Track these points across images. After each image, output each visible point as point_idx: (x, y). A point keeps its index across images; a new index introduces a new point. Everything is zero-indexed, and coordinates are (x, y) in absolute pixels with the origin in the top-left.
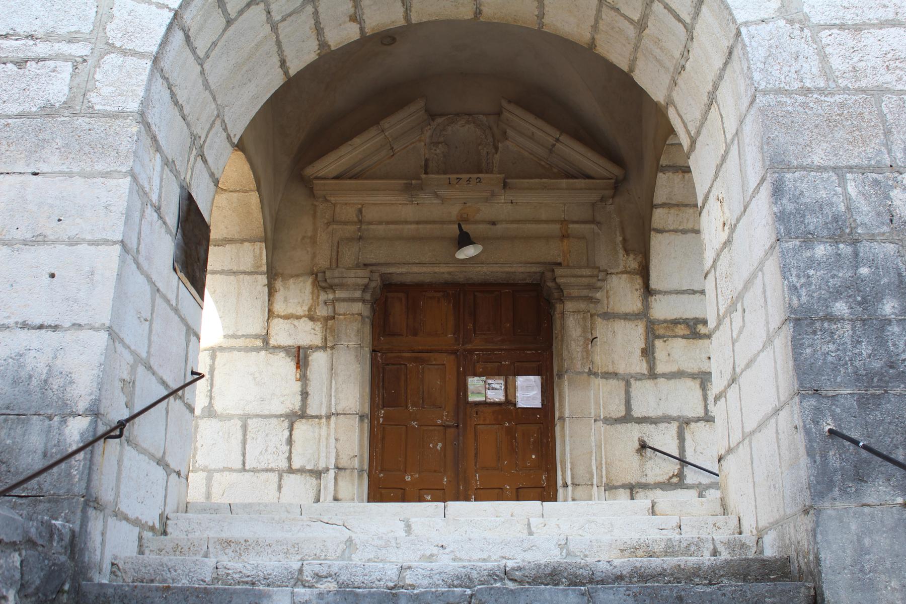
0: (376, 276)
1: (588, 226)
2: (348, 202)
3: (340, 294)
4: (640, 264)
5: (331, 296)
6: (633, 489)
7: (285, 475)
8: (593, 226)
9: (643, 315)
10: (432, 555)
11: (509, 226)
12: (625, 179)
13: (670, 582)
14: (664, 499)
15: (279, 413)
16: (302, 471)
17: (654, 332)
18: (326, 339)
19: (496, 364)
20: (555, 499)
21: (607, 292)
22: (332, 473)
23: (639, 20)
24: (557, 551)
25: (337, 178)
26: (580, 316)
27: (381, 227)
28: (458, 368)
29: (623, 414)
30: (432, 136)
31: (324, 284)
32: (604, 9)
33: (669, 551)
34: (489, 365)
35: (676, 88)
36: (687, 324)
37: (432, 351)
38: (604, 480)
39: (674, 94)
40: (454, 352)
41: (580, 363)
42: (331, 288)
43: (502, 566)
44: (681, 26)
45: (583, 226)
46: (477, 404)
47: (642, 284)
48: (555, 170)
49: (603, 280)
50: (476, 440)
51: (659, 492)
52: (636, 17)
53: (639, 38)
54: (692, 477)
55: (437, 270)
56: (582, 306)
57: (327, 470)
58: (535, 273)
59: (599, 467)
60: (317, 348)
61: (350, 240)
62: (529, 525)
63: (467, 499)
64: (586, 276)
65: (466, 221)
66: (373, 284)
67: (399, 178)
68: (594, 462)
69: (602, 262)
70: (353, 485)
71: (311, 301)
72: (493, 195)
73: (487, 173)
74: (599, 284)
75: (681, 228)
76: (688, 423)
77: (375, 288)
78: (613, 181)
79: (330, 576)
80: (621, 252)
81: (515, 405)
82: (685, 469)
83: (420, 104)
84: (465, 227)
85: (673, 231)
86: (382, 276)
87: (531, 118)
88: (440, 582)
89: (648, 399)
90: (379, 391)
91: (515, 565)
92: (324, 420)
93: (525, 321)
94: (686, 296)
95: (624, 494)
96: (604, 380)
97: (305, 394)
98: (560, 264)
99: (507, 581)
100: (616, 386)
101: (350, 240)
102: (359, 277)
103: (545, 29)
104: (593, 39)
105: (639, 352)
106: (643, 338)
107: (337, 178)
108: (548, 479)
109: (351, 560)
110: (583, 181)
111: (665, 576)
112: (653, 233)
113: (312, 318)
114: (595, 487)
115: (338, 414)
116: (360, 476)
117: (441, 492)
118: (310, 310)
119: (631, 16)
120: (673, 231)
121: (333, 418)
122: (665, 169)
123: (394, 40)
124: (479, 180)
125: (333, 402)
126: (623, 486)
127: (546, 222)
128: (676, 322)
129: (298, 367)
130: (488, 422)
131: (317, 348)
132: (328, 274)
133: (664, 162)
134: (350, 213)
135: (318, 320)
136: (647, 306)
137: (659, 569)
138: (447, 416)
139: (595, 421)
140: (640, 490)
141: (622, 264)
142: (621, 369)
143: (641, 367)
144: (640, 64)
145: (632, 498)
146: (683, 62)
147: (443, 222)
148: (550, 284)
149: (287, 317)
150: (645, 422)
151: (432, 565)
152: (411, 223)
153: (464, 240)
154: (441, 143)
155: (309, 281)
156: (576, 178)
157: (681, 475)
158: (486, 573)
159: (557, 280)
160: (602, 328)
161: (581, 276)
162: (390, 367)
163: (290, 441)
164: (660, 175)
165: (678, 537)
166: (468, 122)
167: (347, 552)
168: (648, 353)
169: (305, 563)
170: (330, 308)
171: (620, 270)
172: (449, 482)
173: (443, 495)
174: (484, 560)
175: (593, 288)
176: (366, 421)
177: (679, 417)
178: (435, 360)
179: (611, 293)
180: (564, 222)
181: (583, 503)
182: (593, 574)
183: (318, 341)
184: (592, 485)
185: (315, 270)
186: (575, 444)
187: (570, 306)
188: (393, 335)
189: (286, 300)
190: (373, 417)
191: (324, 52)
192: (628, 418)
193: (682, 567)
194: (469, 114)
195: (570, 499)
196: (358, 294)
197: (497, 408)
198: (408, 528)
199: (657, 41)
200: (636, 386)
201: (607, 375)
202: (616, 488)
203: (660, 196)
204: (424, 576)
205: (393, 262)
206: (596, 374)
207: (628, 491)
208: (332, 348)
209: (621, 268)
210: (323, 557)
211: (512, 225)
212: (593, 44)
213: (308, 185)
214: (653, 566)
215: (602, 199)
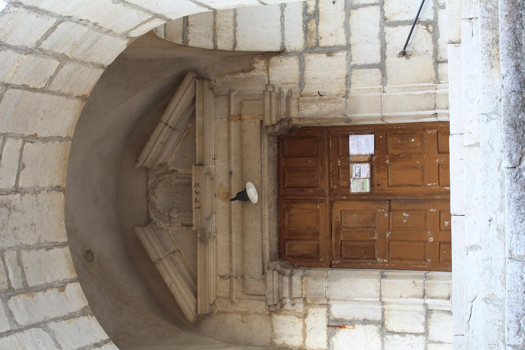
0: (272, 265)
1: (232, 100)
2: (214, 287)
3: (286, 294)
4: (261, 59)
5: (288, 300)
6: (438, 61)
7: (429, 338)
8: (232, 96)
9: (300, 56)
10: (498, 229)
11: (232, 161)
12: (195, 71)
13: (521, 24)
14: (446, 33)
15: (380, 343)
16: (426, 325)
17: (313, 47)
18: (322, 305)
19: (341, 170)
20: (447, 123)
21: (283, 84)
22: (428, 301)
23: (59, 61)
24: (493, 123)
25: (196, 295)
26: (301, 104)
27: (234, 260)
28: (344, 200)
29: (378, 70)
30: (164, 222)
31: (279, 306)
32: (51, 88)
33: (493, 26)
34: (341, 176)
35: (114, 30)
36: (307, 21)
37: (331, 221)
38: (431, 84)
39: (119, 32)
40: (331, 203)
41: (338, 105)
42: (281, 300)
43: (508, 170)
44: (60, 26)
45: (232, 104)
46: (372, 185)
47: (276, 57)
48: (190, 125)
49: (274, 87)
50: (401, 186)
51: (441, 41)
52: (56, 63)
53: (74, 60)
54: (427, 15)
55: (267, 217)
56: (294, 103)
57: (425, 304)
58: (269, 141)
59: (421, 88)
60: (328, 311)
61: (244, 285)
62: (470, 146)
63: (448, 193)
64: (271, 101)
65: (229, 194)
66: (279, 267)
67: (197, 244)
68: (417, 93)
69: (259, 88)
70: (437, 278)
71: (292, 316)
72: (209, 174)
73: (191, 179)
74: (277, 90)
75: (232, 27)
76: (385, 19)
77: (281, 266)
78: (197, 81)
79: (518, 321)
80: (252, 73)
81: (372, 155)
82: (421, 20)
83: (139, 230)
84: (234, 196)
85: (235, 33)
86: (272, 260)
87: (150, 144)
88: (523, 224)
89: (366, 51)
90: (362, 263)
91: (507, 159)
92: (386, 307)
93: (306, 150)
94: (286, 23)
95: (442, 68)
96: (352, 85)
97: (365, 322)
98: (262, 121)
99: (521, 167)
100: (357, 76)
101: (244, 285)
102: (273, 278)
103: (71, 135)
104: (78, 97)
105: (330, 59)
106: (318, 56)
107: (196, 295)
108: (431, 129)
109: (504, 299)
110: (197, 104)
111: (515, 28)
112: (237, 49)
113: (305, 316)
114: (437, 91)
115: (381, 296)
116: (430, 278)
117: (442, 213)
118: (299, 317)
119: (56, 67)
120: (235, 33)
121: (384, 300)
122: (185, 41)
123: (89, 252)
124: (197, 185)
125: (371, 299)
126: (436, 69)
127: (229, 132)
128: (306, 30)
129: (344, 327)
130: (386, 177)
131: (328, 311)
132: (270, 303)
133: (180, 41)
134: (224, 285)
135: (307, 310)
136: (294, 53)
137: (510, 33)
138: (381, 209)
139: (384, 92)
140: (439, 55)
141: (261, 73)
142: (343, 72)
143: (341, 57)
144: (97, 59)
145: (446, 61)
146: (91, 25)
147: (230, 212)
148: (277, 129)
149: (305, 335)
150: (385, 52)
151: (508, 230)
152: (231, 238)
153: (243, 196)
154: (169, 214)
155: (276, 317)
156: (195, 111)
157: (427, 24)
158: (514, 185)
159: (274, 123)
160: (310, 88)
161: (271, 104)
162: (343, 253)
163: (403, 334)
164: (190, 44)
165: (480, 19)
166: (154, 193)
167: (496, 303)
168: (330, 52)
169: (507, 343)
170: (297, 301)
171: (266, 75)
172: (433, 207)
173: (445, 214)
174: (501, 185)
175: (279, 96)
176: (386, 273)
177: (380, 26)
178: (337, 218)
179: (284, 81)
180: (229, 119)
181: (450, 101)
182: (514, 91)
183: (323, 311)
184: (435, 94)
185: (267, 313)
186: (402, 106)
187: (294, 113)
188: (318, 251)
189: (291, 336)
190: (383, 267)
191: (90, 311)
192: (382, 67)
193: (507, 13)
194: (148, 192)
195: (447, 111)
196: (286, 279)
197: (375, 169)
198: (474, 248)
199: (75, 46)
200: (356, 60)
201: (348, 83)
202: (437, 75)
203: (208, 44)
204: (518, 239)
205: (261, 251)
206: (347, 92)
207: (440, 65)
208: (328, 300)
209: (265, 74)
210: (501, 324)
211: (232, 160)
212: (82, 98)
213: (201, 319)
214: (506, 39)
215: (212, 89)
